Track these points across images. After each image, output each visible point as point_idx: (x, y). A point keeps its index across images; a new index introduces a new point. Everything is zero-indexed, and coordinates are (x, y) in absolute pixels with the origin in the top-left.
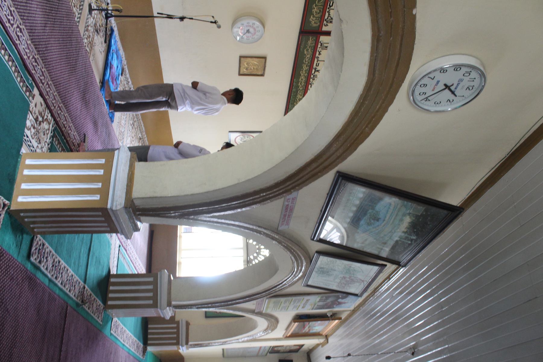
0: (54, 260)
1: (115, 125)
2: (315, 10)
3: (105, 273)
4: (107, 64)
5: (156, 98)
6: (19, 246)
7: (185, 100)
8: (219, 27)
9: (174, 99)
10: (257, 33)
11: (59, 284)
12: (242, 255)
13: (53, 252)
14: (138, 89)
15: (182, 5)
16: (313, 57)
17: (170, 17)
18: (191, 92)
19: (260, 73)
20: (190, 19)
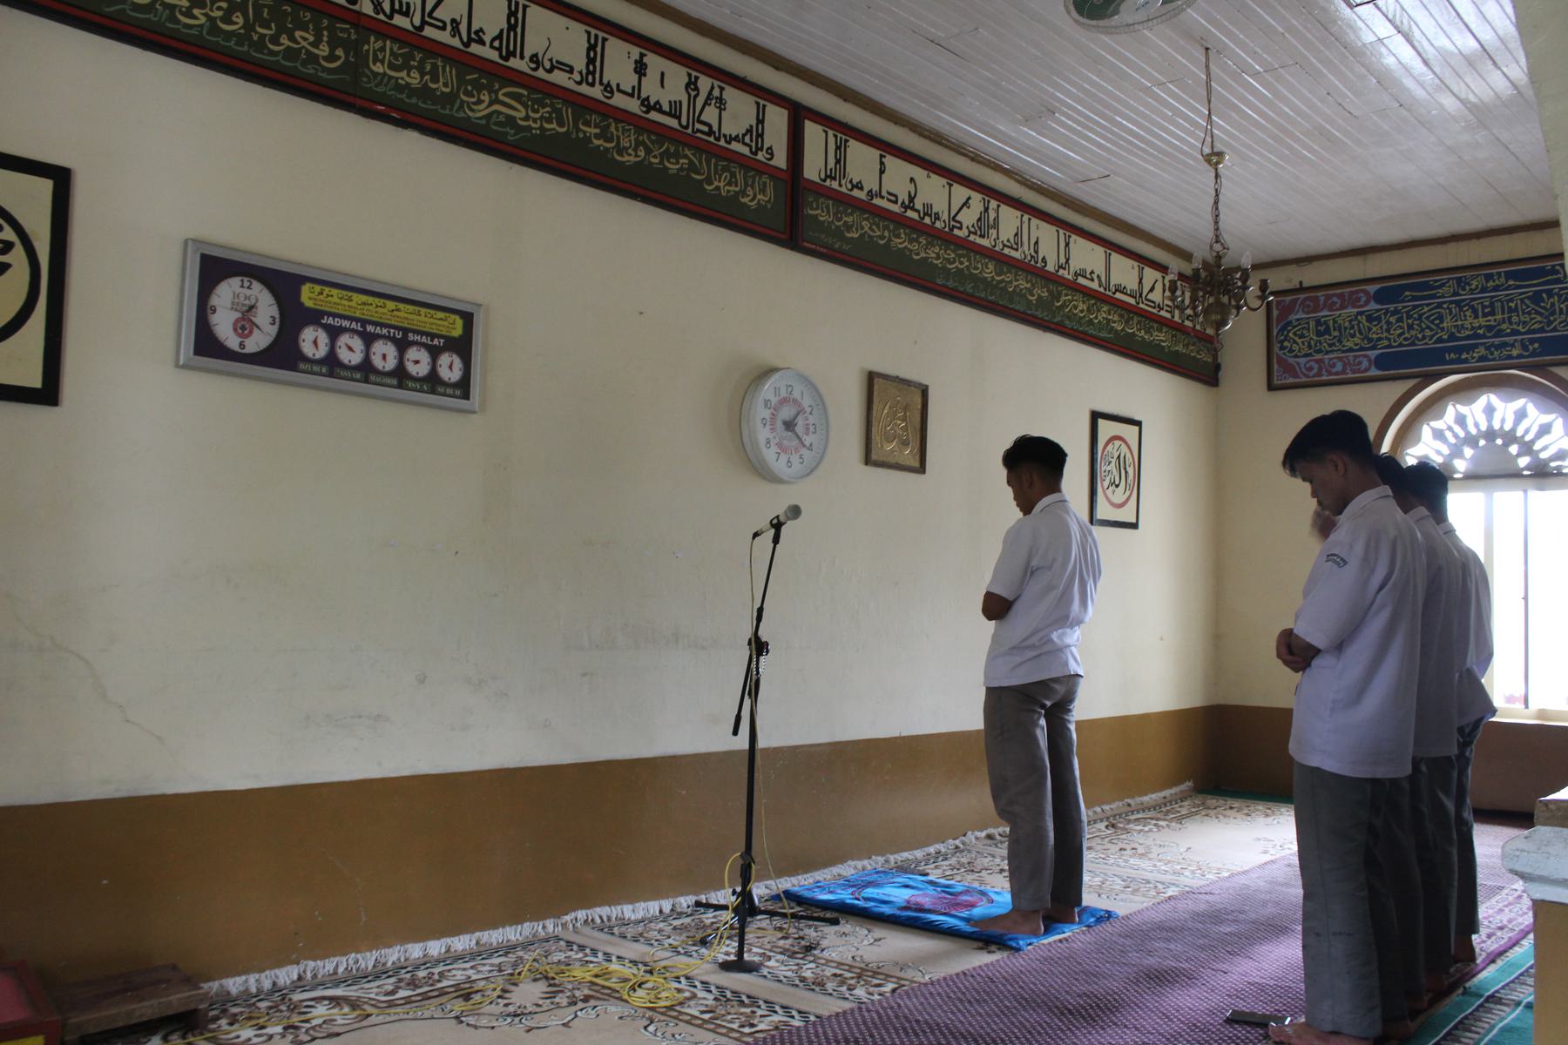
1: (1121, 907)
2: (721, 185)
4: (911, 921)
5: (1030, 751)
7: (1046, 648)
8: (795, 512)
9: (1044, 686)
10: (796, 395)
12: (1519, 494)
14: (1005, 813)
15: (703, 648)
16: (867, 208)
17: (752, 687)
18: (1021, 622)
19: (919, 400)
20: (759, 618)
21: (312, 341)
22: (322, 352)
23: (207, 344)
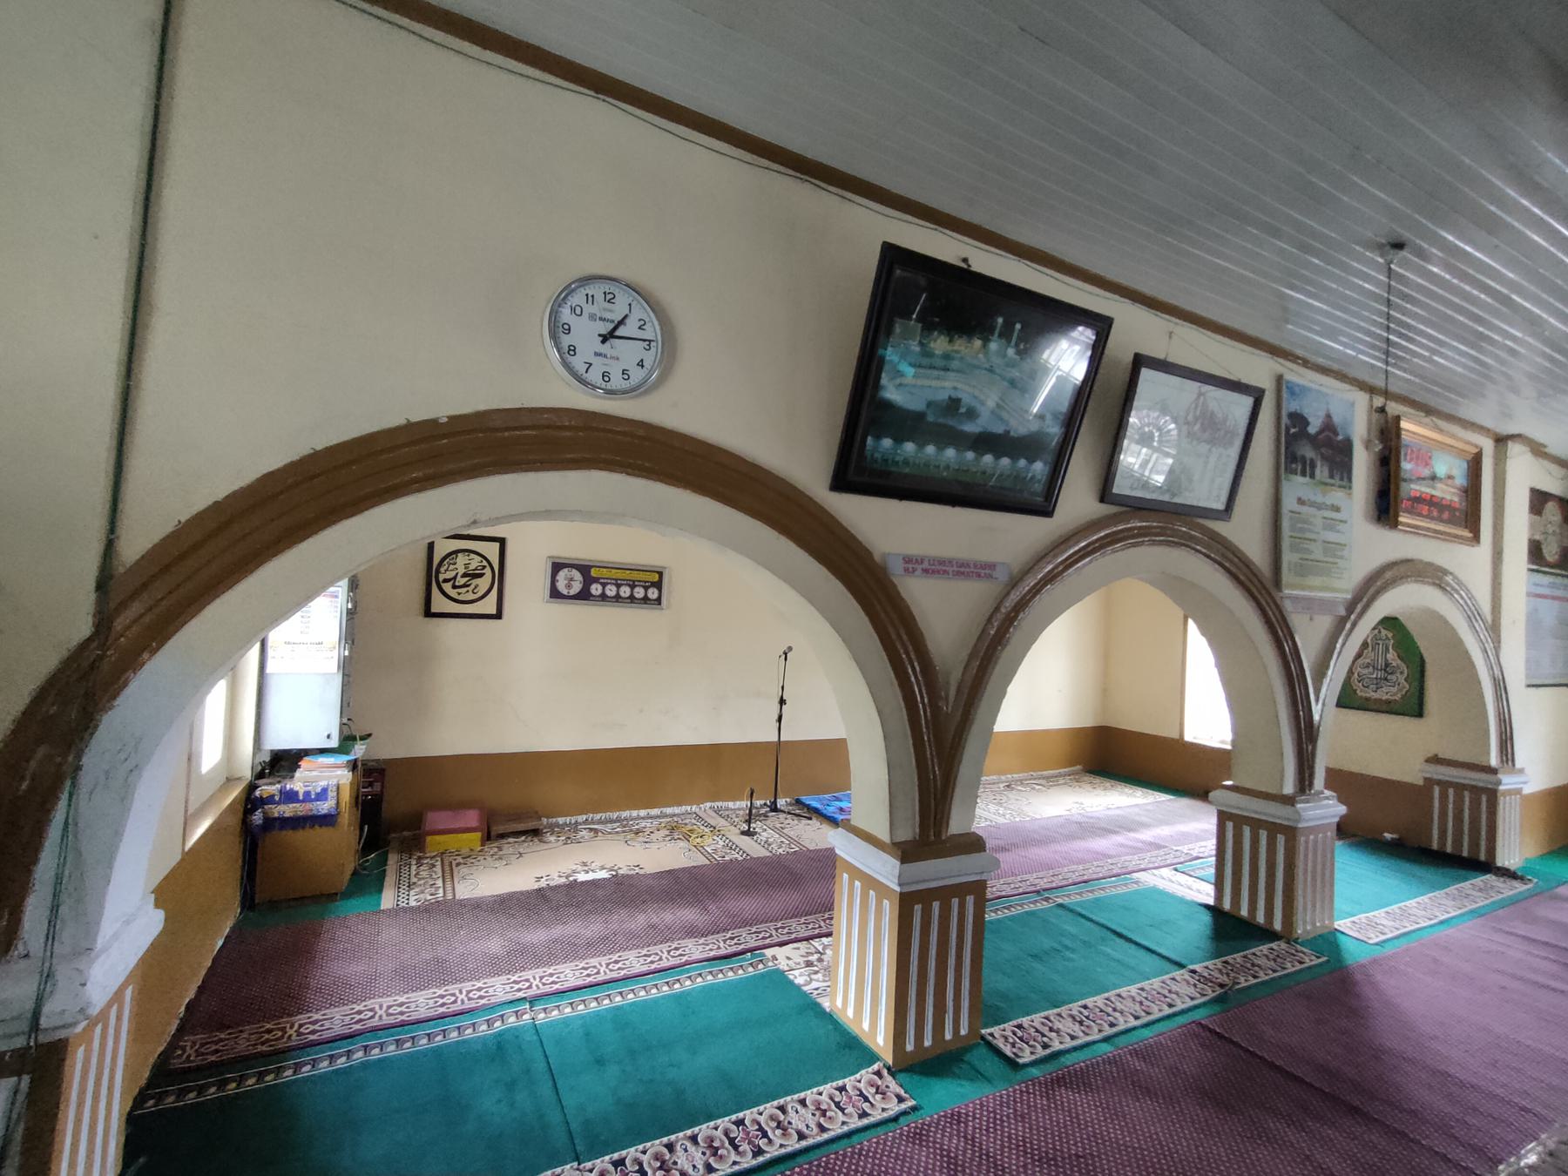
0: (1073, 1017)
3: (1206, 918)
6: (977, 1075)
8: (790, 649)
11: (1133, 1023)
13: (1051, 1012)
21: (596, 589)
22: (600, 592)
23: (555, 594)
